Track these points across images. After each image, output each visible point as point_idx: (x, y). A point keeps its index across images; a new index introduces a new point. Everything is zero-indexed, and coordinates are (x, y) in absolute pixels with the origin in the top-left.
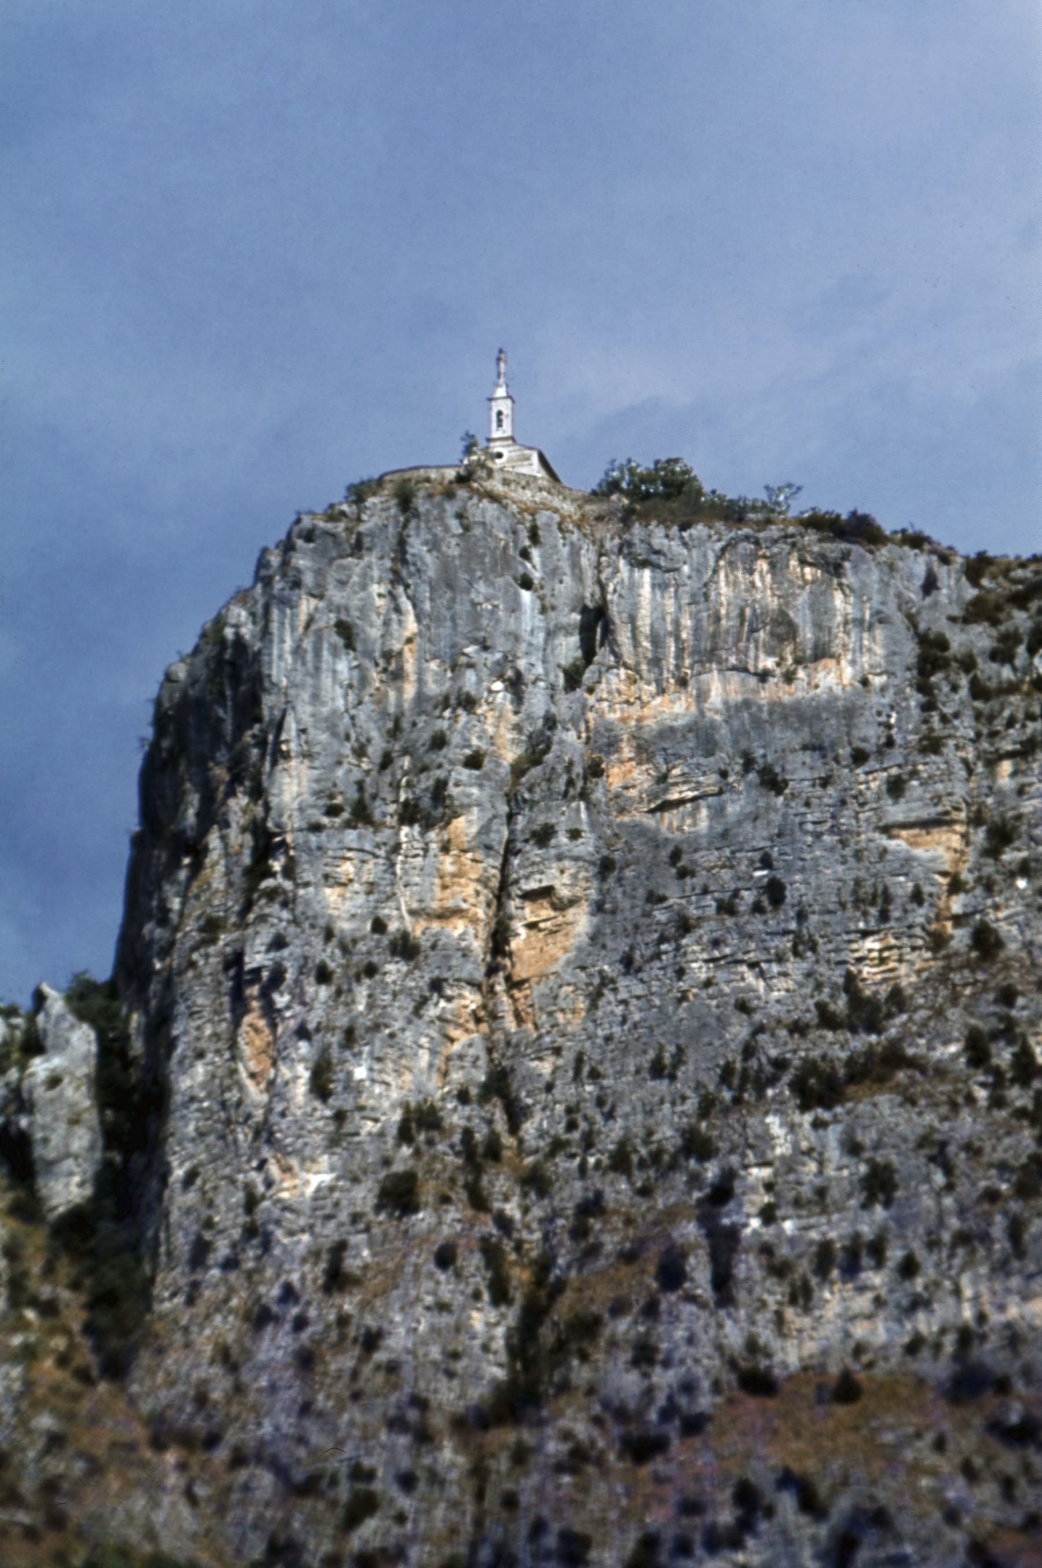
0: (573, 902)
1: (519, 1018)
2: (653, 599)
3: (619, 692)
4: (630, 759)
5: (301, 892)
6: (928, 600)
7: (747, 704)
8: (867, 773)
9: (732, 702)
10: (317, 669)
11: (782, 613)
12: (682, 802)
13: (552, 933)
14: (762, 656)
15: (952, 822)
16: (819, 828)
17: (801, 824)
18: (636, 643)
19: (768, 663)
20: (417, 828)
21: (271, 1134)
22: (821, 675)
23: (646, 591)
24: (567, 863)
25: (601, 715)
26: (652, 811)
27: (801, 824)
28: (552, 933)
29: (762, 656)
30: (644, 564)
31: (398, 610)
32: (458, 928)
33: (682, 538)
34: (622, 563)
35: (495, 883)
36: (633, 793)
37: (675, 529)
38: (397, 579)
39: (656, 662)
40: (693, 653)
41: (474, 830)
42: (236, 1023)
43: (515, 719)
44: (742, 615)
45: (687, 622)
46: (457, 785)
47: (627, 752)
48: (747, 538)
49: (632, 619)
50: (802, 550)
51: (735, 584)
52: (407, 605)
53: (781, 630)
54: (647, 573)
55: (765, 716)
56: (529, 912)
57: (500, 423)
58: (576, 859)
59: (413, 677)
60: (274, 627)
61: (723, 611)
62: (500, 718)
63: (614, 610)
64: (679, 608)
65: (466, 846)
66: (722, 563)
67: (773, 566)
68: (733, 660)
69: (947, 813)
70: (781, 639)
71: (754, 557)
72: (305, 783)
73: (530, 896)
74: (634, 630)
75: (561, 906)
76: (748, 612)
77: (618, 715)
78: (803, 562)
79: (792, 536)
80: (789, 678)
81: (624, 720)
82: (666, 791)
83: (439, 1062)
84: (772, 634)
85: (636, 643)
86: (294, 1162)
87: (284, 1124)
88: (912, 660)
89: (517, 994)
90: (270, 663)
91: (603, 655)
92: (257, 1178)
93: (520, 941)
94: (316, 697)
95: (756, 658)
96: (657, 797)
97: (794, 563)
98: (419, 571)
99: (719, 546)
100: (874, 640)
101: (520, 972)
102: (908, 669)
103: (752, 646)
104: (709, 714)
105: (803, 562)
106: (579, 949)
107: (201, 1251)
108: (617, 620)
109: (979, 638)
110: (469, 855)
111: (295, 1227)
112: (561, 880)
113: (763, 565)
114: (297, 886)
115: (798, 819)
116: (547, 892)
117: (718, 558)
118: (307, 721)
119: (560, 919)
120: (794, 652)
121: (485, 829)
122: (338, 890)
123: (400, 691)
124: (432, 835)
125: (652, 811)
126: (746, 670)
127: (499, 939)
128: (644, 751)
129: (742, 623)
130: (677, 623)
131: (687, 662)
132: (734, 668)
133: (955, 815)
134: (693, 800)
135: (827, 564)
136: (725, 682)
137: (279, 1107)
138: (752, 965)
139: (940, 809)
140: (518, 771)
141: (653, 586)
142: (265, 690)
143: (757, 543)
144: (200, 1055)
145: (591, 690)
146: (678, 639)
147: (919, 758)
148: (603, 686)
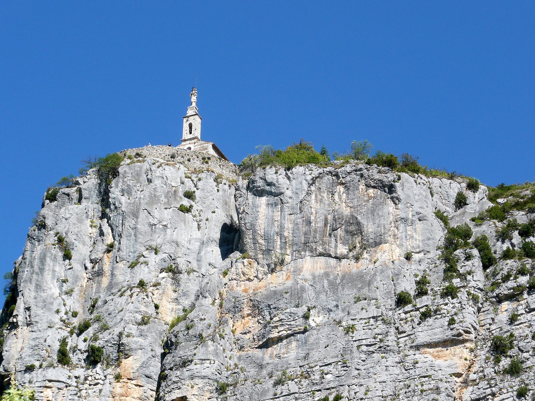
3: (244, 274)
4: (249, 315)
6: (459, 212)
8: (406, 313)
9: (317, 273)
10: (42, 270)
12: (280, 339)
14: (340, 245)
15: (465, 341)
16: (371, 349)
17: (359, 347)
19: (342, 250)
22: (378, 255)
24: (196, 380)
27: (359, 347)
29: (340, 245)
33: (287, 174)
37: (282, 171)
39: (268, 252)
43: (175, 295)
44: (326, 220)
45: (289, 225)
46: (128, 336)
47: (247, 311)
49: (253, 225)
53: (353, 228)
54: (264, 200)
55: (338, 281)
57: (190, 126)
58: (204, 377)
61: (312, 218)
65: (132, 376)
66: (313, 188)
68: (320, 249)
69: (460, 335)
70: (352, 234)
76: (330, 217)
77: (243, 287)
78: (368, 186)
79: (361, 170)
81: (245, 291)
84: (347, 232)
88: (442, 243)
94: (38, 287)
95: (336, 246)
96: (264, 337)
97: (362, 187)
98: (116, 208)
102: (438, 248)
103: (333, 239)
104: (300, 282)
105: (368, 186)
109: (489, 229)
110: (134, 382)
115: (356, 344)
117: (310, 185)
118: (32, 303)
123: (99, 283)
124: (109, 371)
125: (260, 347)
126: (330, 256)
129: (326, 225)
130: (282, 227)
131: (288, 251)
132: (321, 255)
133: (465, 336)
134: (287, 336)
135: (384, 186)
139: (455, 332)
143: (337, 175)
146: (281, 236)
147: (441, 301)
148: (233, 269)
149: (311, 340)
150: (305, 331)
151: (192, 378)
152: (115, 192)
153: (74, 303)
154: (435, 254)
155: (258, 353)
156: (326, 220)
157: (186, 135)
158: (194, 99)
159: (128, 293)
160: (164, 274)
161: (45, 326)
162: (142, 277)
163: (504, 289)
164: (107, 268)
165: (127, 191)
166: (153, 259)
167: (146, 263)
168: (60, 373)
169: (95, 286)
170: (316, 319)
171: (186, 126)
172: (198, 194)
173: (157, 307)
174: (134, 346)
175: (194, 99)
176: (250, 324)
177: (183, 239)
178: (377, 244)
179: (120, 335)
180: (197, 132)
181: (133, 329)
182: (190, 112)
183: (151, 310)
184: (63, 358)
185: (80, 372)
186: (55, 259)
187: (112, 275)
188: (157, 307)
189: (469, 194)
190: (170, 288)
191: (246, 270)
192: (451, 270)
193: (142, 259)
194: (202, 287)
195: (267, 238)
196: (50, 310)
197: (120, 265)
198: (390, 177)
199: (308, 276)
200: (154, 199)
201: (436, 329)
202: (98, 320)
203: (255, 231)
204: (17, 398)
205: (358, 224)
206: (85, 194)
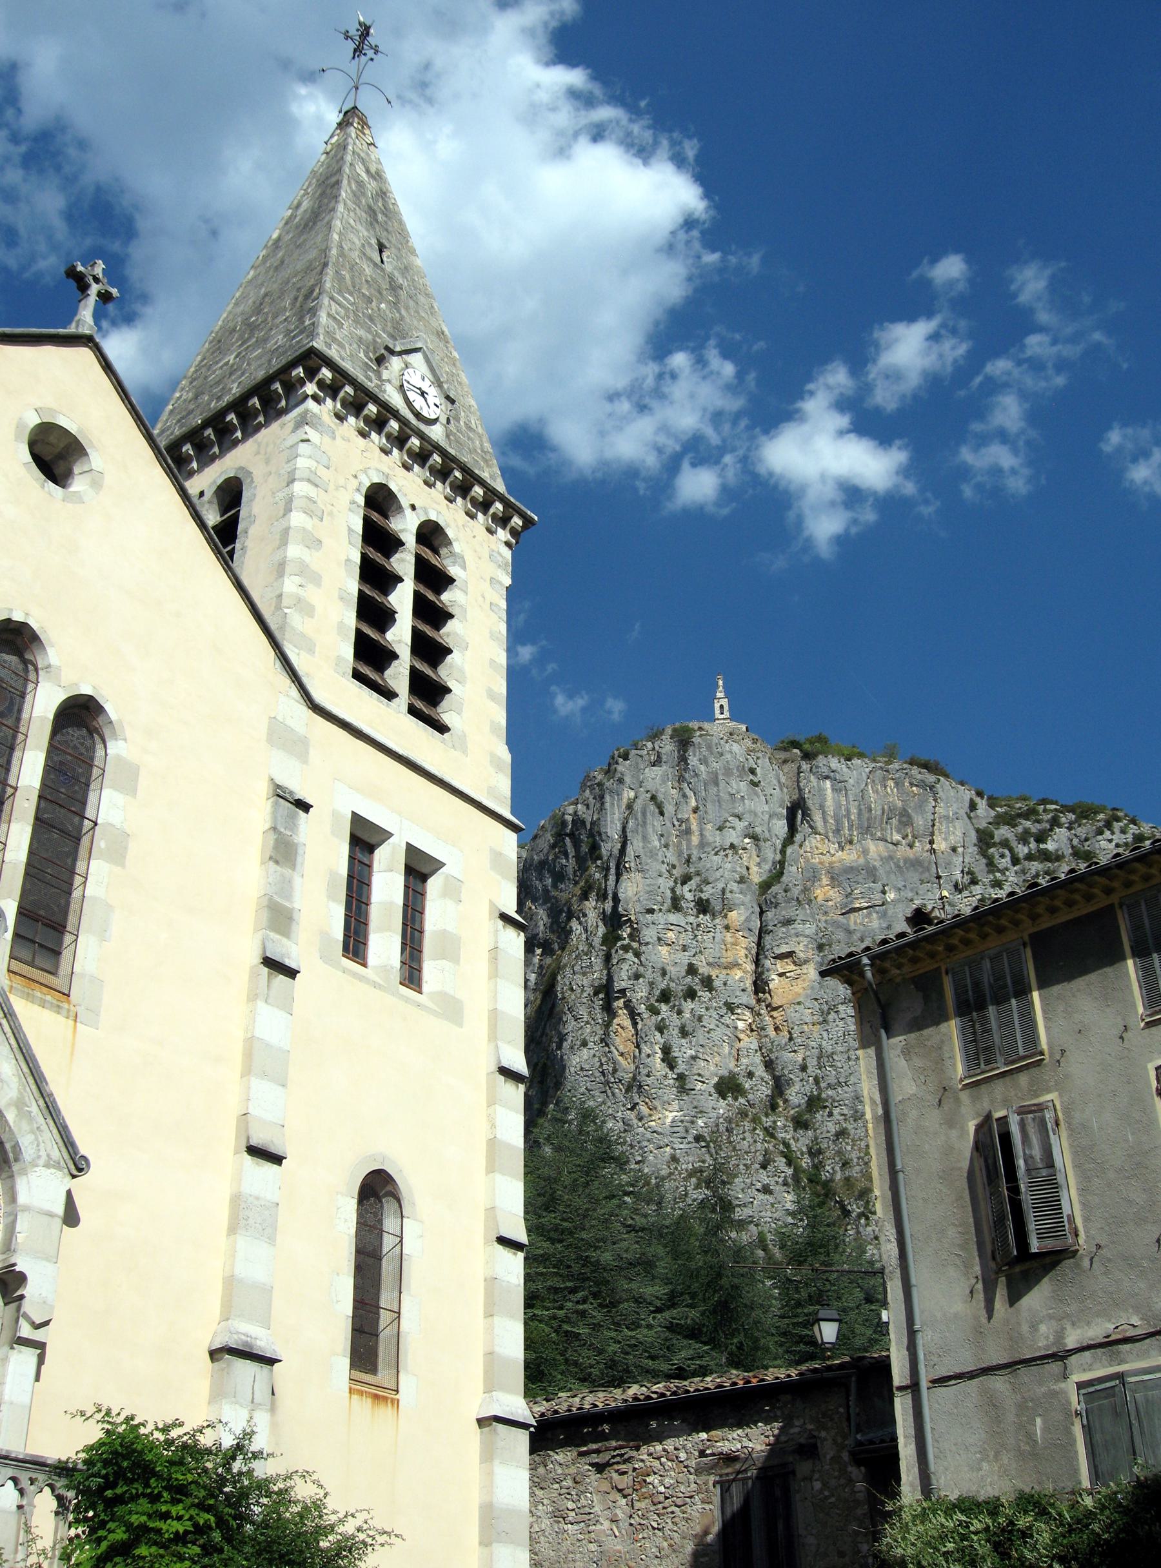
0: (806, 962)
1: (777, 1029)
2: (833, 798)
5: (644, 948)
7: (891, 858)
10: (645, 823)
11: (905, 810)
12: (861, 909)
19: (897, 837)
20: (708, 917)
21: (640, 1086)
23: (829, 791)
24: (801, 938)
25: (807, 860)
30: (827, 777)
31: (685, 796)
32: (738, 974)
34: (812, 778)
35: (754, 951)
38: (681, 779)
39: (837, 831)
40: (857, 828)
41: (743, 918)
42: (607, 1025)
44: (883, 810)
48: (881, 768)
49: (822, 806)
50: (911, 777)
51: (877, 792)
53: (904, 819)
54: (828, 782)
56: (781, 966)
57: (722, 707)
58: (807, 936)
59: (697, 833)
60: (607, 805)
62: (750, 857)
63: (810, 803)
64: (848, 803)
67: (897, 784)
68: (879, 834)
71: (885, 779)
72: (640, 886)
74: (824, 813)
78: (912, 784)
80: (911, 846)
82: (852, 902)
83: (734, 1052)
84: (900, 821)
85: (825, 821)
86: (657, 1103)
87: (649, 1081)
89: (775, 1014)
90: (606, 826)
91: (803, 829)
92: (632, 1116)
93: (775, 982)
97: (907, 784)
99: (867, 770)
100: (955, 827)
101: (776, 1002)
106: (812, 988)
108: (812, 808)
111: (662, 1143)
112: (802, 949)
113: (891, 783)
114: (641, 944)
116: (790, 954)
118: (641, 852)
119: (799, 972)
120: (912, 831)
121: (748, 920)
122: (666, 948)
123: (689, 841)
124: (717, 921)
127: (760, 986)
128: (834, 880)
129: (883, 813)
130: (848, 811)
134: (866, 908)
136: (877, 846)
137: (644, 1071)
140: (765, 886)
141: (833, 790)
144: (584, 1044)
145: (801, 846)
149: (890, 912)
150: (883, 904)
151: (797, 935)
152: (693, 761)
153: (671, 857)
154: (973, 850)
156: (883, 810)
157: (718, 715)
158: (721, 683)
159: (722, 853)
160: (747, 840)
161: (655, 874)
162: (731, 840)
164: (694, 826)
165: (704, 761)
166: (740, 825)
167: (733, 828)
168: (674, 918)
169: (684, 843)
170: (891, 896)
171: (717, 706)
172: (758, 770)
173: (748, 869)
174: (737, 902)
175: (721, 683)
177: (759, 810)
179: (723, 891)
180: (727, 714)
181: (734, 886)
182: (719, 695)
183: (745, 872)
184: (676, 905)
185: (691, 919)
186: (653, 815)
187: (701, 835)
188: (748, 869)
189: (978, 800)
190: (754, 853)
191: (819, 845)
192: (991, 865)
193: (728, 824)
194: (96, 737)
196: (657, 860)
197: (709, 826)
198: (931, 778)
199: (875, 856)
200: (728, 772)
202: (698, 874)
205: (909, 816)
206: (664, 758)
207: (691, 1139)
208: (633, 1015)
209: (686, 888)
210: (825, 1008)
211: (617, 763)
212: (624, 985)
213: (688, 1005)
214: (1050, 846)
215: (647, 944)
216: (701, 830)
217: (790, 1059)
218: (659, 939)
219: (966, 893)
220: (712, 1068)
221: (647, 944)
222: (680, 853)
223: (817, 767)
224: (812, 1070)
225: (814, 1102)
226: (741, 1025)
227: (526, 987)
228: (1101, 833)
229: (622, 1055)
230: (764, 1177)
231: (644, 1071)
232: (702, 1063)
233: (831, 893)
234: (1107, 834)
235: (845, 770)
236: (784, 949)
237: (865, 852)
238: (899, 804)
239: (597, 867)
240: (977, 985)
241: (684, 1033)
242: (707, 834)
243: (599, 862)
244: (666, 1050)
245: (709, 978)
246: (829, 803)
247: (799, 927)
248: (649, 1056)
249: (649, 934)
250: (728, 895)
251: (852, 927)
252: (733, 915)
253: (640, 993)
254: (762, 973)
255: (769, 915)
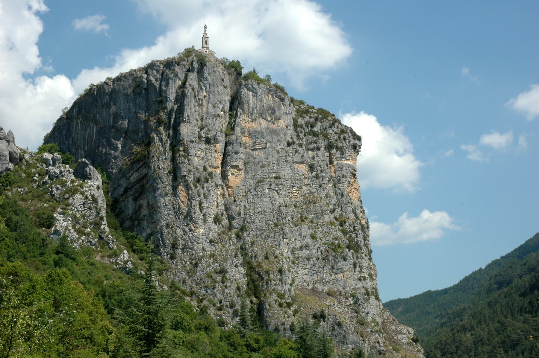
9: (205, 67)
12: (258, 149)
13: (237, 176)
18: (249, 109)
23: (251, 96)
26: (252, 150)
28: (237, 176)
36: (247, 144)
39: (252, 114)
49: (248, 102)
52: (204, 88)
53: (273, 112)
56: (233, 171)
59: (206, 107)
60: (170, 85)
73: (232, 167)
75: (239, 170)
78: (276, 96)
82: (255, 145)
85: (249, 109)
107: (174, 246)
113: (270, 96)
123: (202, 109)
130: (257, 106)
134: (260, 149)
138: (276, 191)
142: (168, 101)
143: (270, 90)
146: (257, 110)
155: (251, 152)
163: (311, 147)
164: (205, 103)
176: (248, 140)
178: (279, 119)
187: (207, 108)
195: (253, 109)
197: (210, 105)
201: (297, 158)
203: (249, 105)
204: (337, 357)
205: (275, 111)
207: (208, 241)
208: (187, 188)
209: (202, 132)
210: (247, 190)
211: (174, 66)
212: (185, 173)
213: (206, 185)
214: (315, 129)
215: (191, 156)
216: (207, 106)
217: (235, 209)
218: (196, 154)
219: (291, 147)
220: (212, 211)
221: (191, 156)
222: (199, 114)
223: (248, 85)
224: (242, 215)
225: (243, 229)
226: (219, 193)
227: (370, 252)
228: (331, 127)
229: (182, 202)
230: (235, 261)
231: (193, 212)
232: (210, 209)
233: (248, 140)
234: (333, 128)
235: (258, 88)
236: (235, 164)
237: (260, 124)
238: (272, 105)
239: (164, 112)
240: (106, 109)
241: (205, 197)
242: (209, 107)
243: (165, 110)
244: (200, 204)
245: (211, 173)
246: (251, 101)
247: (240, 155)
248: (195, 206)
249: (192, 152)
250: (217, 137)
251: (255, 156)
252: (218, 145)
253: (191, 179)
254: (225, 172)
255: (229, 148)
